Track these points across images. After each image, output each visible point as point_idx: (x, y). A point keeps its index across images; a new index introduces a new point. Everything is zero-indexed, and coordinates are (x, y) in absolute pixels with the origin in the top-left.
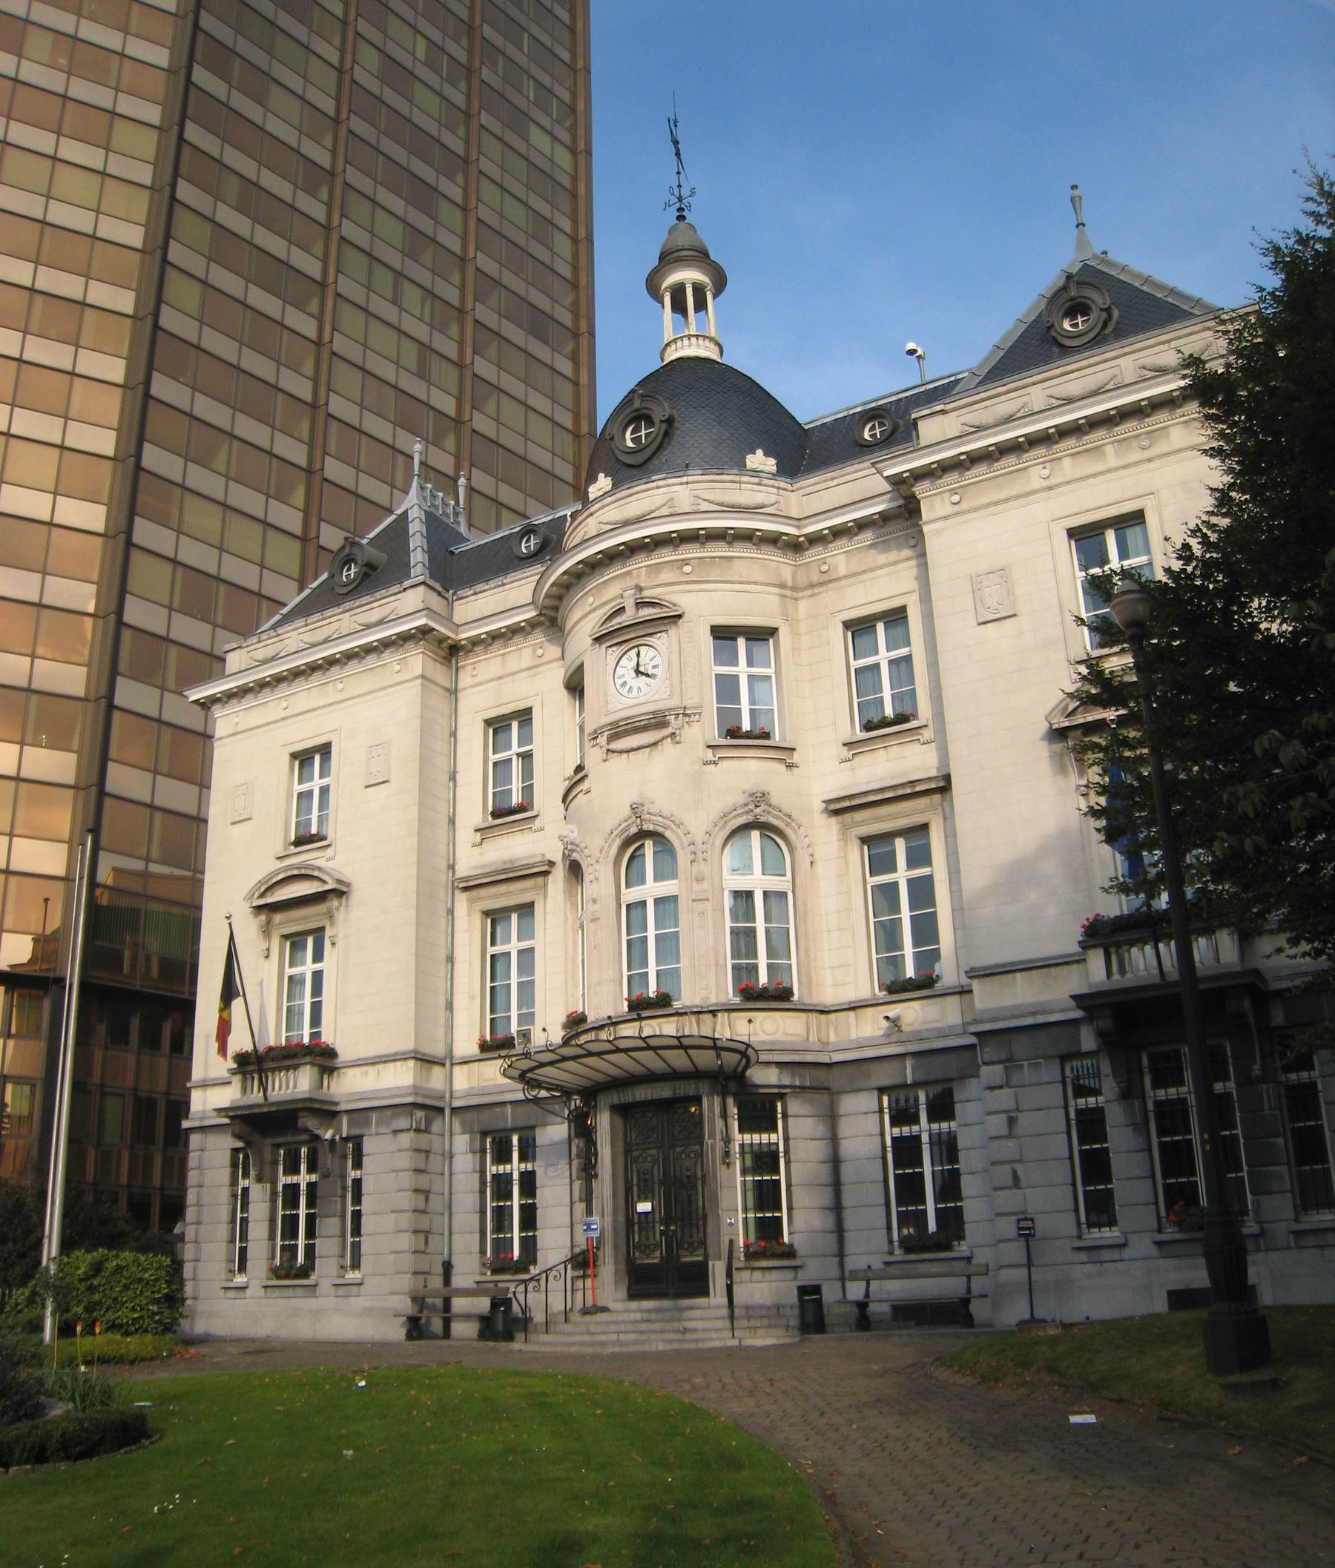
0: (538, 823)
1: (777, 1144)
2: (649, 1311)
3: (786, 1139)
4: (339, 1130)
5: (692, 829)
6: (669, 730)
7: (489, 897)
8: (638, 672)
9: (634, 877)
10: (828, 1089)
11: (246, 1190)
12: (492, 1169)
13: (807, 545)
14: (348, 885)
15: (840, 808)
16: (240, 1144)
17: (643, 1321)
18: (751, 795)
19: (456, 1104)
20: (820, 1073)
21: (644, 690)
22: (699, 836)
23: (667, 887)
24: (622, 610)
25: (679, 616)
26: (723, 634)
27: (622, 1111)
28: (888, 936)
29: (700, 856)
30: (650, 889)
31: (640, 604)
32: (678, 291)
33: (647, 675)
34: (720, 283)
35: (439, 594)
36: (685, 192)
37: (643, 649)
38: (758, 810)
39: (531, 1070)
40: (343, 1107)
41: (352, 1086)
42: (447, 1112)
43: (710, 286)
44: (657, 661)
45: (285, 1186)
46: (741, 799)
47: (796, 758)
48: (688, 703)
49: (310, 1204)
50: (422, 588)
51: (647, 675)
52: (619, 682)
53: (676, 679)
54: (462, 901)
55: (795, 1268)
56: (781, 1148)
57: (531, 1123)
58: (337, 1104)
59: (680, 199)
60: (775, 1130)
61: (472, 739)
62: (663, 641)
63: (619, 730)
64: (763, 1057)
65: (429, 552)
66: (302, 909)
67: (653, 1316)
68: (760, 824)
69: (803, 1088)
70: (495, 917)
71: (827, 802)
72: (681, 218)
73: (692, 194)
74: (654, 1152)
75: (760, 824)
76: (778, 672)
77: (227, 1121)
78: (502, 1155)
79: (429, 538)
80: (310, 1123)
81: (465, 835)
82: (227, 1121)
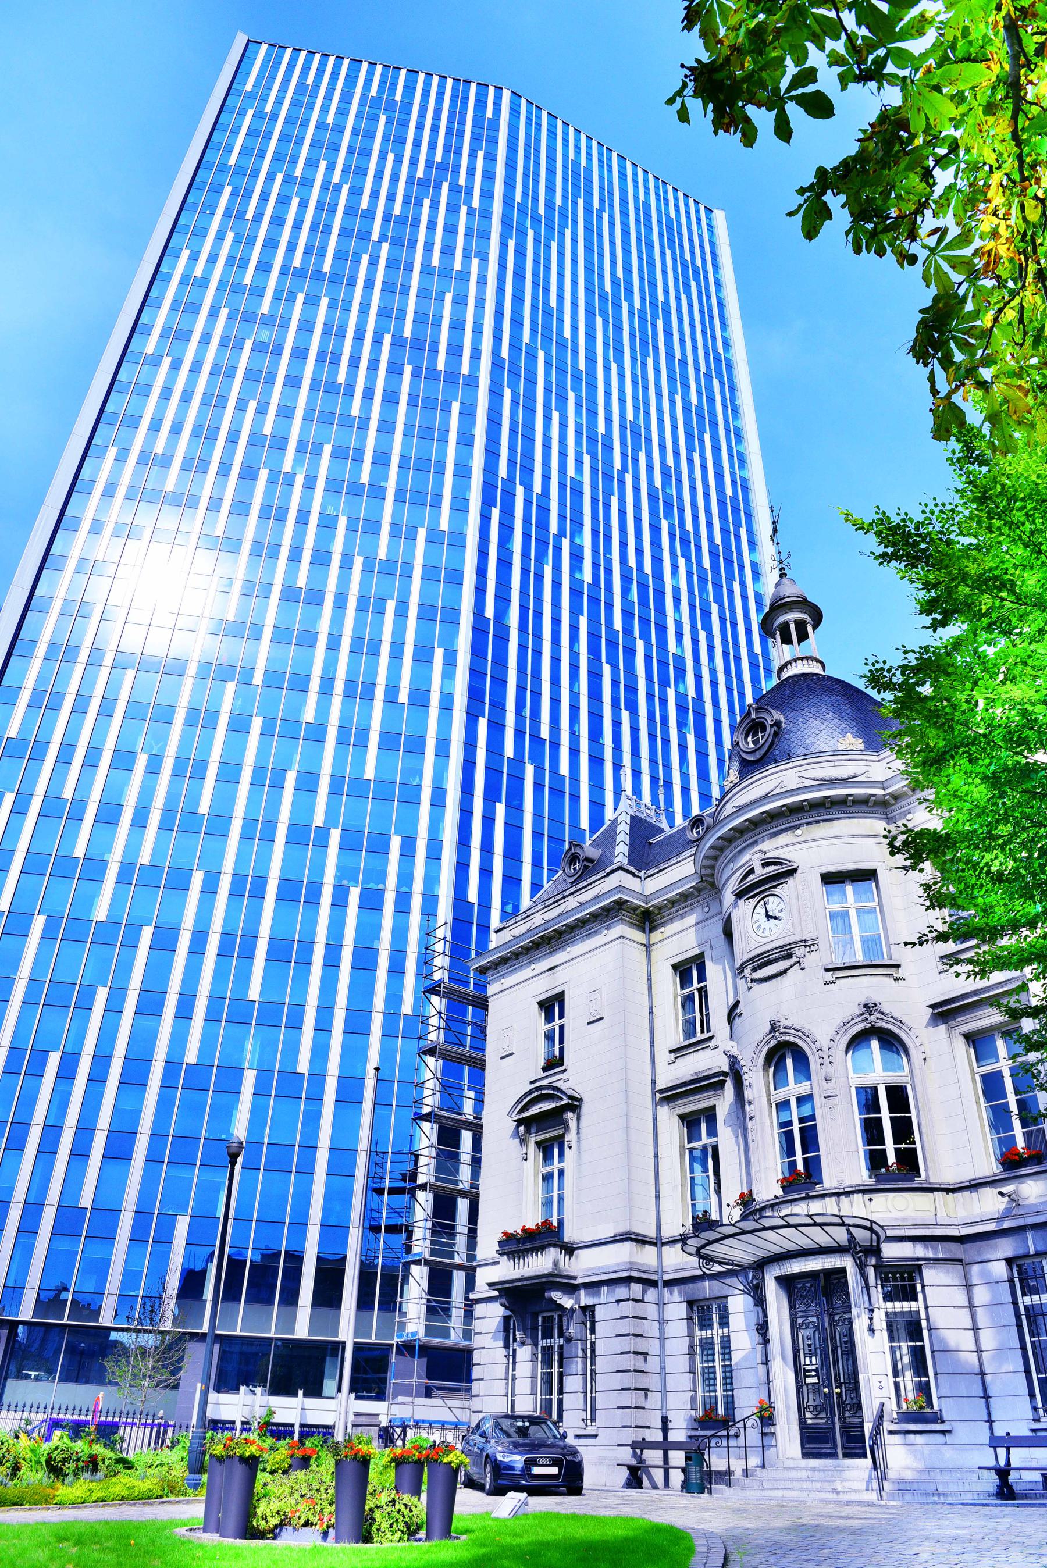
0: (712, 1044)
1: (918, 1312)
2: (813, 1470)
3: (1015, 1303)
4: (577, 1301)
5: (818, 1038)
6: (794, 960)
7: (683, 1105)
8: (768, 917)
9: (780, 1081)
10: (961, 1260)
11: (514, 1351)
12: (698, 1334)
13: (892, 801)
14: (580, 1100)
15: (945, 1012)
16: (509, 1313)
17: (808, 1479)
18: (866, 1006)
19: (666, 1277)
20: (954, 1246)
21: (774, 929)
22: (824, 1043)
23: (803, 1088)
24: (752, 871)
25: (795, 870)
26: (830, 879)
27: (786, 1282)
28: (999, 1119)
29: (826, 1060)
30: (794, 1088)
31: (765, 865)
32: (785, 629)
33: (775, 918)
34: (817, 617)
35: (634, 875)
36: (784, 556)
37: (771, 898)
38: (872, 1018)
39: (703, 1247)
40: (580, 1281)
41: (584, 1266)
42: (660, 1284)
43: (809, 620)
44: (782, 906)
45: (701, 1340)
46: (858, 1011)
47: (901, 973)
48: (807, 937)
49: (560, 1366)
50: (620, 872)
51: (775, 918)
52: (755, 926)
53: (796, 920)
54: (663, 1111)
55: (943, 1432)
56: (923, 1316)
57: (724, 1294)
58: (575, 1278)
59: (781, 562)
60: (916, 1300)
61: (667, 984)
62: (787, 889)
63: (762, 961)
64: (890, 1233)
65: (630, 845)
66: (547, 1120)
67: (817, 1475)
68: (878, 1034)
69: (937, 1260)
70: (690, 1122)
71: (933, 1006)
72: (782, 575)
73: (789, 556)
74: (814, 1319)
75: (878, 1034)
76: (880, 905)
77: (496, 1293)
78: (706, 1324)
79: (632, 835)
80: (555, 1295)
81: (663, 1056)
82: (496, 1293)
